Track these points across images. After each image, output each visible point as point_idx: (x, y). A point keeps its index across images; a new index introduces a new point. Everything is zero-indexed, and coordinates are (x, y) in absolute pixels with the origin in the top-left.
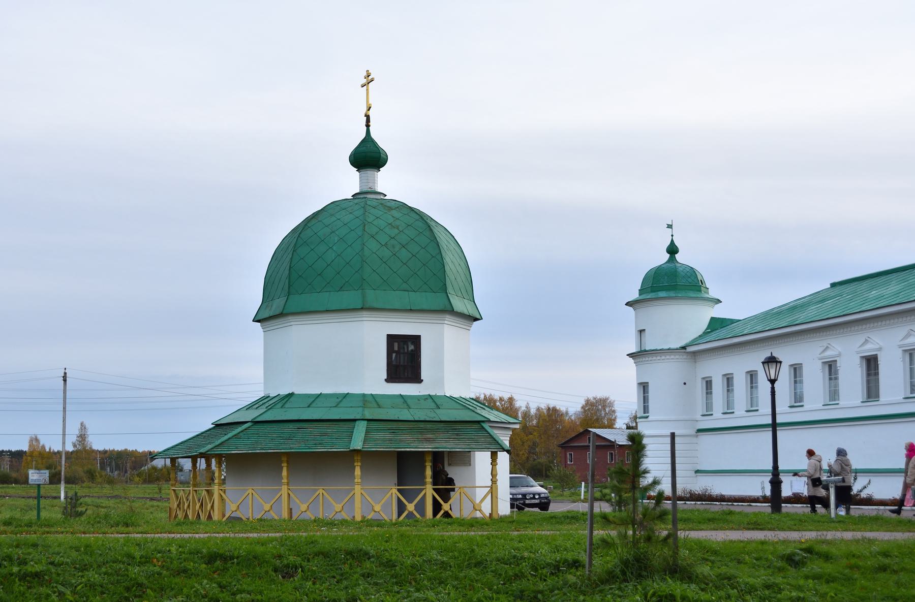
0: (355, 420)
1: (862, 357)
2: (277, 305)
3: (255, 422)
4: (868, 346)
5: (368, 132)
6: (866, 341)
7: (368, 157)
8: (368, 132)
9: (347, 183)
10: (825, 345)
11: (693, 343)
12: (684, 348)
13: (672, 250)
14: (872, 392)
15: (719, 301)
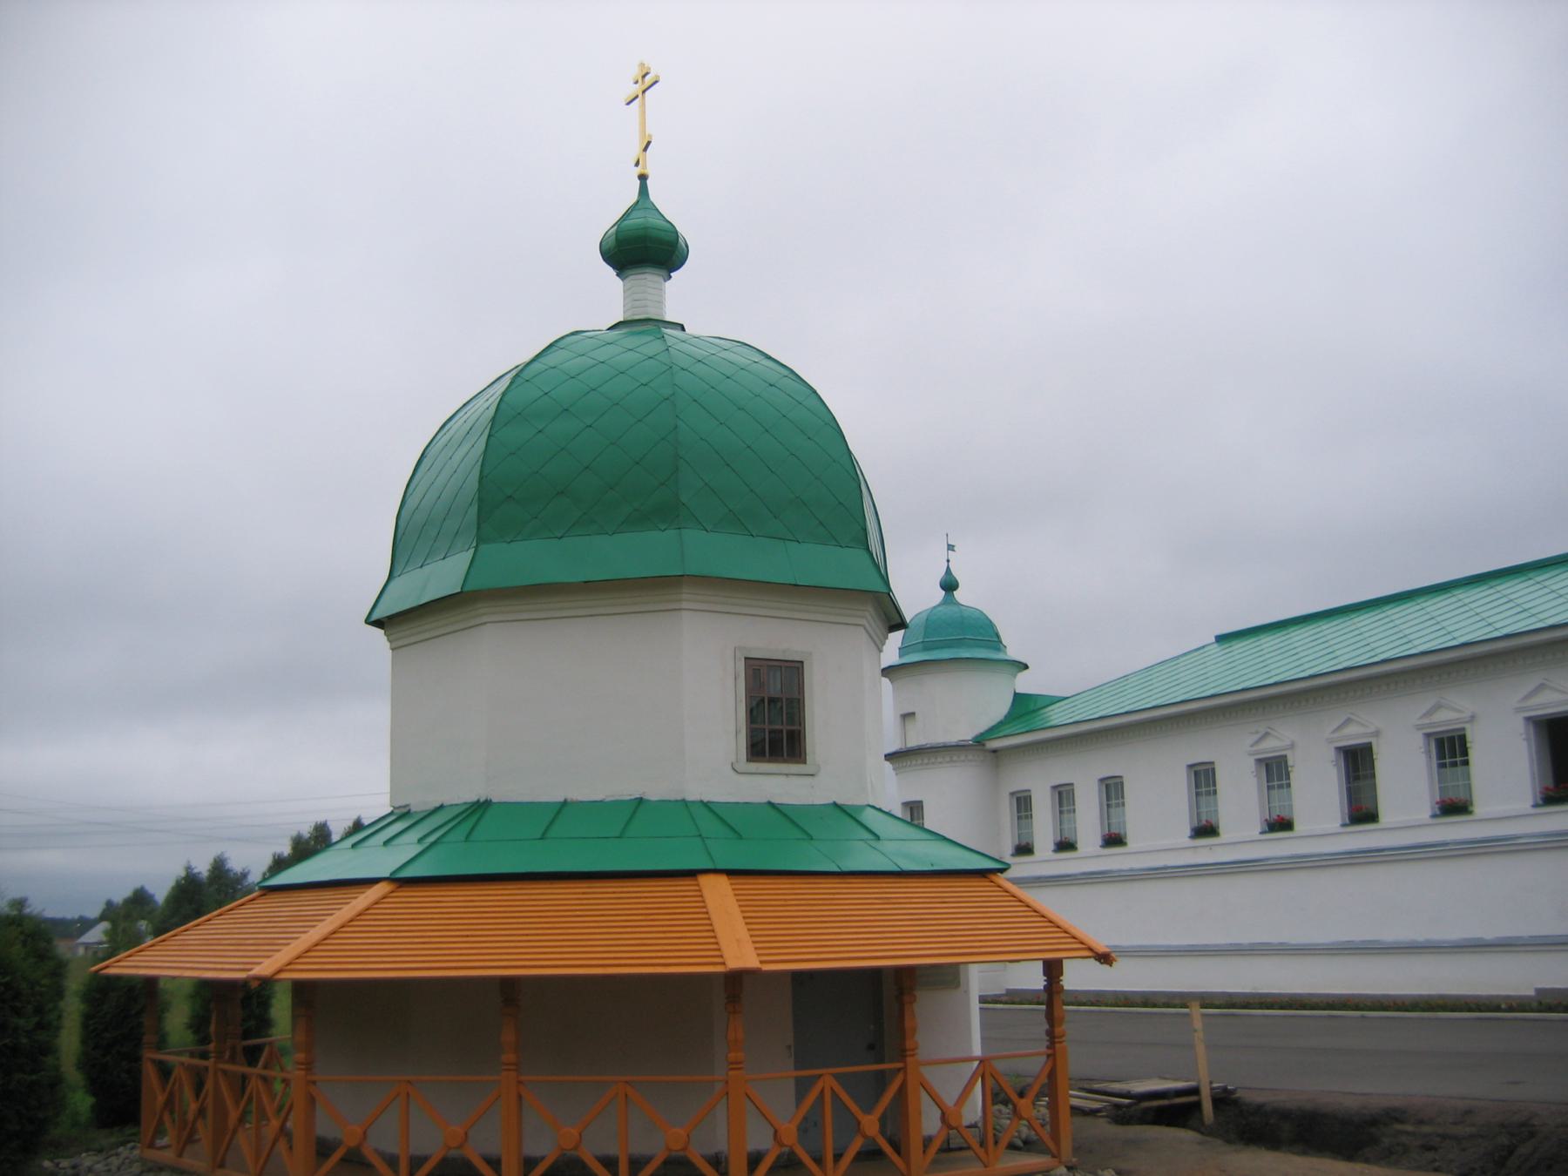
0: (692, 874)
1: (1338, 749)
2: (445, 574)
3: (401, 882)
4: (1352, 730)
5: (643, 190)
6: (1348, 721)
7: (644, 249)
8: (643, 190)
9: (604, 298)
10: (1262, 730)
11: (993, 731)
12: (979, 741)
13: (949, 585)
14: (1362, 813)
15: (1026, 667)
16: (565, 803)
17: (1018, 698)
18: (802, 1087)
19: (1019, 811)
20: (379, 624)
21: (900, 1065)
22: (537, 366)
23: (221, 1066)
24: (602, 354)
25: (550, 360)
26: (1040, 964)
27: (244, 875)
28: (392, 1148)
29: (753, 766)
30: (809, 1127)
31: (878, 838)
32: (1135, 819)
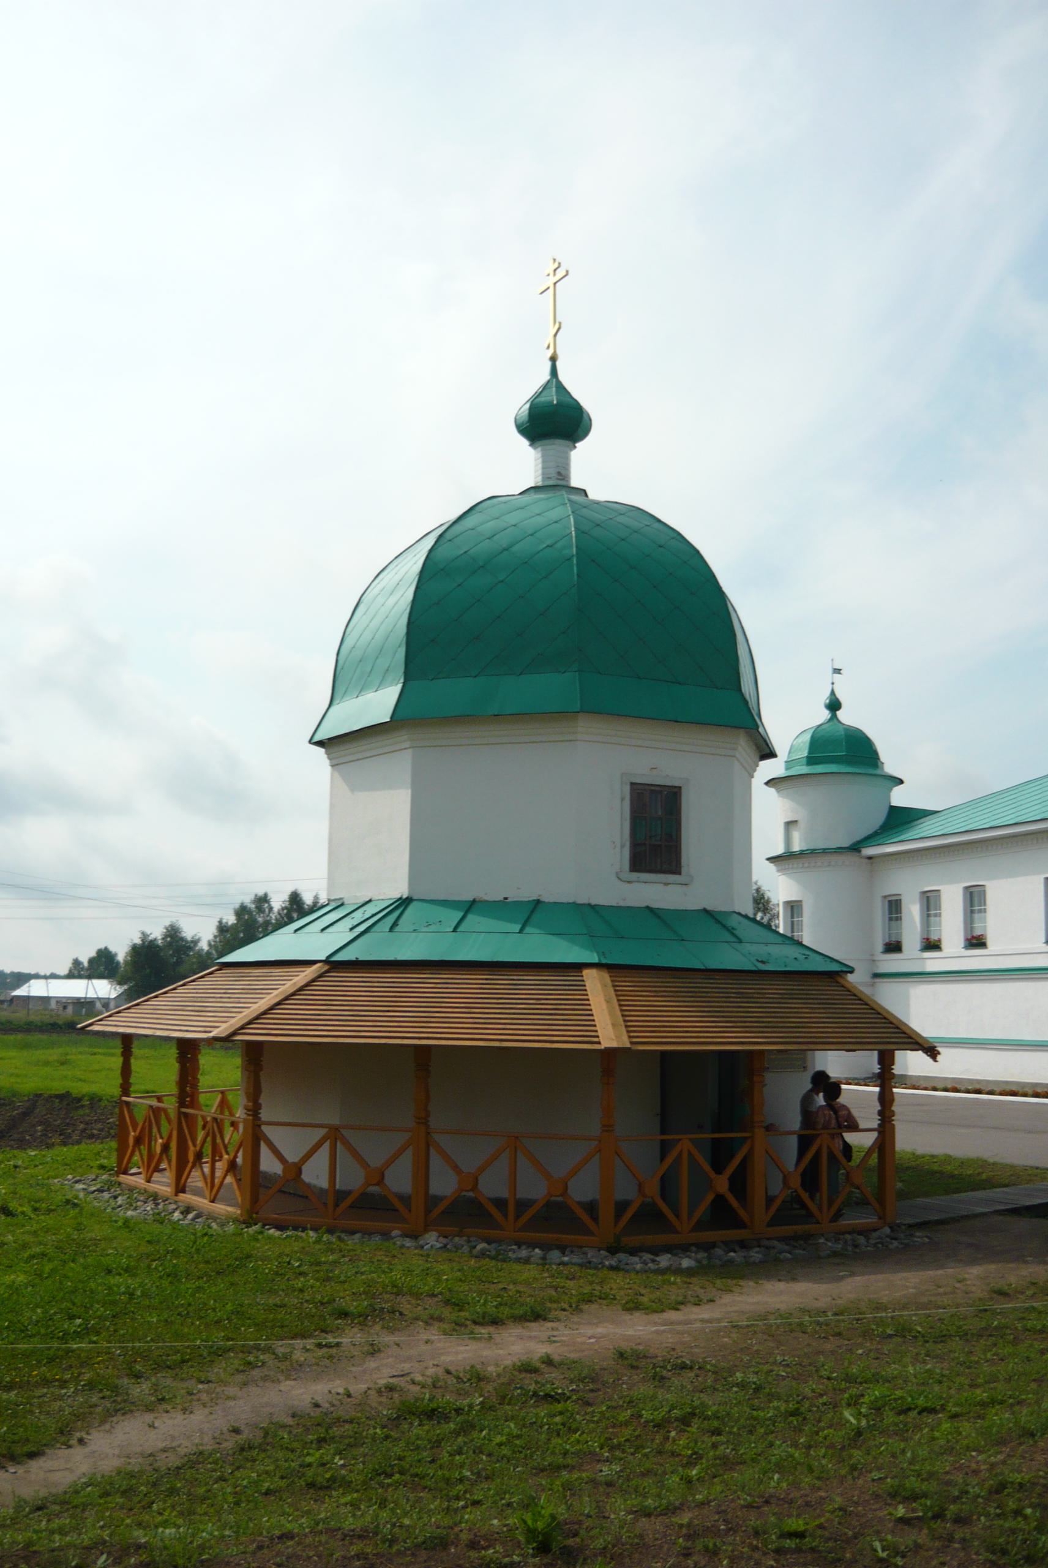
3: (333, 965)
5: (554, 372)
8: (554, 372)
9: (518, 466)
12: (855, 848)
15: (901, 782)
16: (474, 901)
17: (894, 811)
18: (665, 1149)
19: (890, 913)
20: (320, 744)
21: (747, 1135)
22: (458, 528)
23: (183, 1110)
24: (512, 519)
25: (469, 522)
26: (876, 1053)
27: (196, 942)
28: (504, 1193)
29: (635, 875)
30: (667, 1184)
31: (740, 941)
32: (992, 926)
